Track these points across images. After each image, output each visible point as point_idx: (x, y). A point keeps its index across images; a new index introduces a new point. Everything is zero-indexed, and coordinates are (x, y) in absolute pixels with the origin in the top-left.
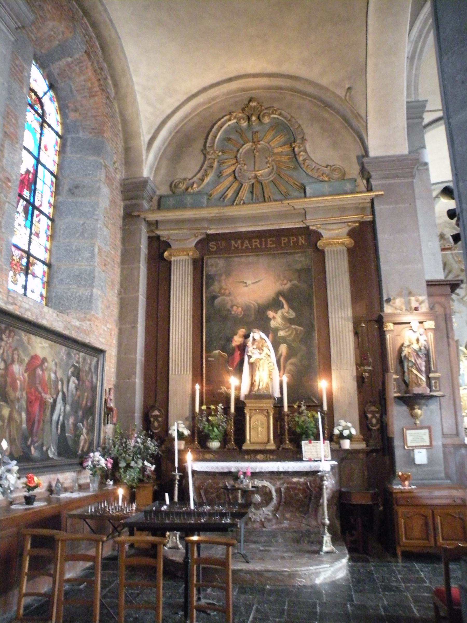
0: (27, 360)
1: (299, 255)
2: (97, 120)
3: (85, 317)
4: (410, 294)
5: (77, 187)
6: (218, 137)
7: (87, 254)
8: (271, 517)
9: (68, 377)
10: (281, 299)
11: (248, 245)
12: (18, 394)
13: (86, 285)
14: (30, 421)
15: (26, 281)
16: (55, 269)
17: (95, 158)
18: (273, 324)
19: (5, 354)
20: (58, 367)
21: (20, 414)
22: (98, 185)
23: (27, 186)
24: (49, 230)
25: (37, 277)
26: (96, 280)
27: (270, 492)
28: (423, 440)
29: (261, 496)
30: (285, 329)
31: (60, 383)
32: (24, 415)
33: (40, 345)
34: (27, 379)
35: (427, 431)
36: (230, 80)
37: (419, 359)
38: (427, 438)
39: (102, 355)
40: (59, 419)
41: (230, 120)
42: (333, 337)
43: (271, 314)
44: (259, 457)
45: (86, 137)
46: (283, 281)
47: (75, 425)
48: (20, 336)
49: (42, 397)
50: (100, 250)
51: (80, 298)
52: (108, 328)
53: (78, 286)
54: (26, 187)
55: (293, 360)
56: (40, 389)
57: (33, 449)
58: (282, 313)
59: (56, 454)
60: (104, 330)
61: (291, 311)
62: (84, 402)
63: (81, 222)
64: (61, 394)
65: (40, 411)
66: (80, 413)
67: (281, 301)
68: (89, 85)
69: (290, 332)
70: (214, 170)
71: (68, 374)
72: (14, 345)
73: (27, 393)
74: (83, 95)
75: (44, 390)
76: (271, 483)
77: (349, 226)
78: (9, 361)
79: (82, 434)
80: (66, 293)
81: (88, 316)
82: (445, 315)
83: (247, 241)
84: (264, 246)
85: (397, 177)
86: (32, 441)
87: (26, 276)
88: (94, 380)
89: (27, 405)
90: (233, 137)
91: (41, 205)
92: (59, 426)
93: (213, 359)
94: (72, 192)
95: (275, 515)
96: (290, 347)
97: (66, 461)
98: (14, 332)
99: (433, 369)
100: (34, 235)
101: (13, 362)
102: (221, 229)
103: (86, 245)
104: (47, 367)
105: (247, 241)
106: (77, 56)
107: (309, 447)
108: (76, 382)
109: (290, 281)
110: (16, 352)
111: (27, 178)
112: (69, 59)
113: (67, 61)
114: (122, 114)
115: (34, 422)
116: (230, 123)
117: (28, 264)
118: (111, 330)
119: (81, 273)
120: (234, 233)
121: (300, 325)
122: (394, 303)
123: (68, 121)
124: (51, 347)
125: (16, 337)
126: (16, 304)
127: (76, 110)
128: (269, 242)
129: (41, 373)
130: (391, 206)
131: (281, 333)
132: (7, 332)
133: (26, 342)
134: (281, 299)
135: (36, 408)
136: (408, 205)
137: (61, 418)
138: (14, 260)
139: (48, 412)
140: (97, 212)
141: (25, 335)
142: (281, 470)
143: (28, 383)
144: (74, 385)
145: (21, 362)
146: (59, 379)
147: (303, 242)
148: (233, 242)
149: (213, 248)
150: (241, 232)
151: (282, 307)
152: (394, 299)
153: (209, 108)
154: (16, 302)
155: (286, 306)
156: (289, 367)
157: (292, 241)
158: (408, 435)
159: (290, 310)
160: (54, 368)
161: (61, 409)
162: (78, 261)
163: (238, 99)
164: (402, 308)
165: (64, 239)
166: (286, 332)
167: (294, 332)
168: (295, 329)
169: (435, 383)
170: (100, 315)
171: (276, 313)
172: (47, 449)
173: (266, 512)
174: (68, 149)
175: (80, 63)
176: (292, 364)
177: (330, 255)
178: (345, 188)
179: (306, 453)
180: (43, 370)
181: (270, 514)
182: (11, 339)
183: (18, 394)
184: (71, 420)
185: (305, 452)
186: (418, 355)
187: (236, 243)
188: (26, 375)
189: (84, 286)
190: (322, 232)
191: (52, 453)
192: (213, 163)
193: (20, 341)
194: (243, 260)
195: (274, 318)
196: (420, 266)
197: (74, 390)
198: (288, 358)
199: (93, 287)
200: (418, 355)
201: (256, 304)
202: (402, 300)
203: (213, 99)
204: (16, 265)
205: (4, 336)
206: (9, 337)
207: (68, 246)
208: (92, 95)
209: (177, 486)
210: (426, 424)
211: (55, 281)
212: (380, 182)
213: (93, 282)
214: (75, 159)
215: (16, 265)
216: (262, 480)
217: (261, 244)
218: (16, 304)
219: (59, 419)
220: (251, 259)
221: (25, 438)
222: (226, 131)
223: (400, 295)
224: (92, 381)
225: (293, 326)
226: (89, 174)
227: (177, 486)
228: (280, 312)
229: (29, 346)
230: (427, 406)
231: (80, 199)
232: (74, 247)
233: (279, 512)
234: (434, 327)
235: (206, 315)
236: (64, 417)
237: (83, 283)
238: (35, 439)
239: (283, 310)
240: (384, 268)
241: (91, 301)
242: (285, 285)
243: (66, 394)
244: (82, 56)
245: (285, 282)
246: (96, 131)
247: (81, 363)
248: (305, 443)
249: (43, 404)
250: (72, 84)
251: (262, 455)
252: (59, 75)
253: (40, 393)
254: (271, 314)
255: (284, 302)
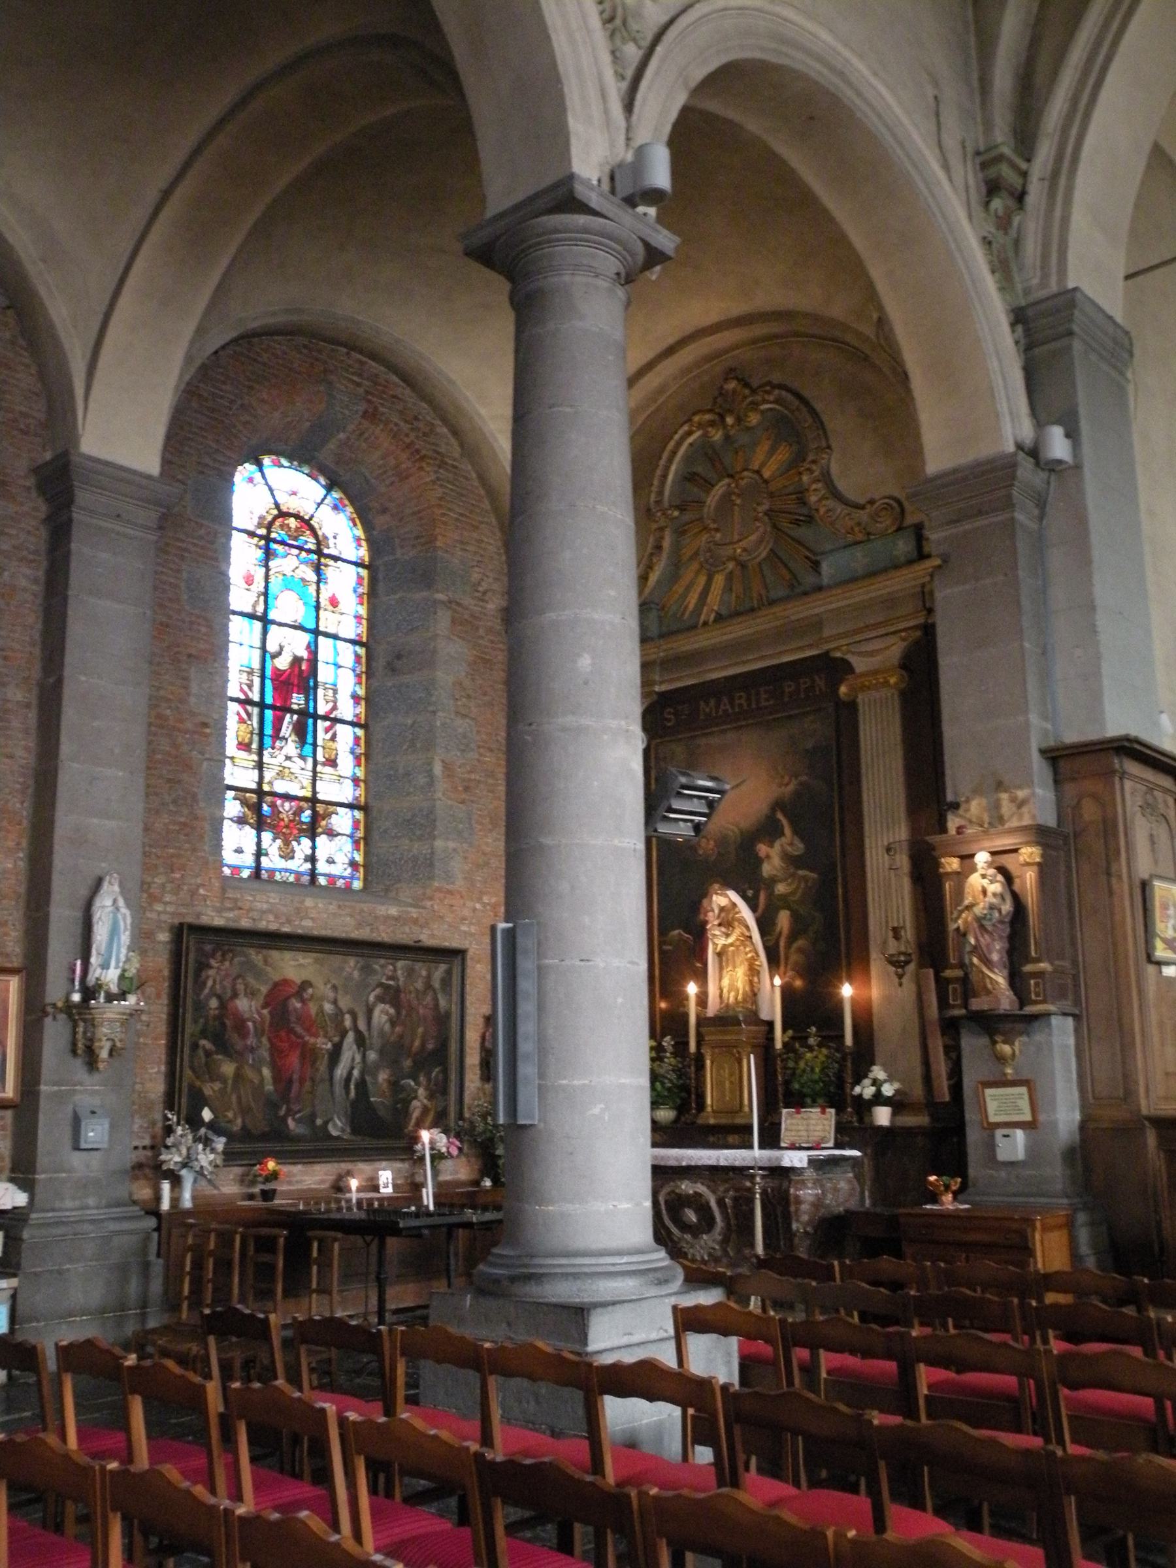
0: (264, 989)
1: (811, 718)
2: (421, 519)
3: (424, 894)
4: (1000, 786)
5: (399, 657)
6: (670, 477)
7: (422, 780)
8: (719, 1253)
9: (367, 1005)
10: (780, 816)
11: (728, 707)
12: (251, 1041)
13: (422, 835)
14: (282, 1079)
15: (314, 848)
16: (374, 813)
17: (425, 594)
18: (767, 870)
19: (218, 987)
20: (340, 992)
21: (260, 1072)
22: (433, 644)
23: (298, 686)
24: (358, 745)
25: (339, 834)
26: (438, 823)
27: (708, 1203)
28: (1019, 1111)
29: (696, 1212)
30: (786, 880)
31: (347, 1017)
32: (266, 1072)
33: (292, 963)
34: (268, 1017)
35: (1023, 1090)
36: (670, 351)
37: (986, 936)
38: (1025, 1104)
39: (460, 957)
40: (350, 1074)
41: (689, 433)
42: (873, 889)
43: (762, 849)
44: (731, 1139)
45: (406, 557)
46: (782, 777)
47: (394, 1085)
48: (246, 956)
49: (305, 1044)
50: (446, 766)
51: (415, 859)
52: (484, 905)
53: (411, 841)
54: (295, 689)
55: (800, 943)
56: (299, 1030)
57: (291, 1123)
58: (782, 846)
59: (348, 1130)
60: (475, 910)
61: (797, 841)
62: (417, 1043)
63: (410, 722)
64: (350, 1037)
65: (302, 1064)
66: (408, 1063)
67: (779, 820)
68: (393, 462)
69: (794, 886)
70: (665, 555)
71: (367, 1001)
72: (235, 971)
73: (269, 1039)
74: (387, 482)
75: (308, 1030)
76: (708, 1187)
77: (903, 639)
78: (229, 993)
79: (415, 1098)
80: (393, 854)
81: (429, 892)
82: (1104, 821)
83: (725, 700)
84: (754, 706)
85: (980, 513)
86: (289, 1111)
87: (313, 841)
88: (442, 1003)
89: (272, 1055)
90: (699, 469)
91: (335, 708)
92: (352, 1087)
93: (669, 948)
94: (392, 669)
95: (725, 1251)
96: (796, 917)
97: (369, 1142)
98: (231, 951)
99: (1033, 954)
100: (324, 764)
101: (235, 995)
102: (678, 679)
103: (419, 763)
104: (312, 996)
105: (725, 700)
106: (351, 427)
107: (794, 1121)
108: (392, 1011)
109: (796, 777)
110: (240, 981)
111: (296, 671)
112: (342, 436)
113: (340, 440)
114: (482, 478)
115: (290, 1081)
116: (691, 440)
117: (315, 818)
118: (494, 907)
119: (414, 816)
120: (704, 683)
121: (812, 870)
122: (968, 810)
123: (375, 533)
124: (316, 960)
125: (236, 960)
126: (240, 909)
127: (384, 511)
128: (764, 696)
129: (298, 1005)
130: (967, 587)
131: (781, 888)
132: (219, 954)
133: (261, 964)
134: (780, 816)
135: (294, 1060)
136: (1001, 577)
137: (356, 1073)
138: (283, 820)
139: (323, 1066)
140: (434, 699)
141: (258, 953)
142: (723, 1163)
143: (271, 1025)
144: (385, 1018)
145: (252, 993)
146: (345, 1010)
147: (824, 689)
148: (702, 703)
149: (669, 720)
150: (713, 681)
151: (782, 834)
152: (968, 801)
153: (657, 410)
154: (239, 904)
155: (788, 831)
156: (794, 957)
157: (803, 686)
158: (988, 1100)
159: (788, 842)
160: (331, 995)
161: (353, 1059)
162: (408, 794)
163: (706, 378)
164: (983, 822)
165: (385, 756)
166: (789, 885)
167: (803, 885)
168: (804, 877)
169: (1037, 984)
170: (460, 884)
171: (772, 846)
172: (326, 1123)
173: (711, 1244)
174: (381, 587)
175: (361, 434)
176: (800, 950)
177: (867, 708)
178: (895, 553)
179: (788, 1133)
180: (303, 1001)
181: (717, 1247)
182: (227, 963)
183: (462, 725)
184: (383, 1076)
185: (786, 1129)
186: (982, 927)
187: (707, 703)
188: (265, 1012)
189: (420, 838)
190: (854, 660)
191: (337, 1127)
192: (662, 538)
193: (250, 966)
194: (715, 741)
195: (768, 857)
196: (1021, 718)
197: (387, 1027)
198: (793, 936)
199: (434, 838)
200: (982, 927)
201: (736, 830)
202: (984, 801)
203: (661, 390)
204: (287, 827)
205: (213, 962)
206: (222, 962)
207: (391, 768)
208: (403, 477)
209: (758, 1196)
210: (1025, 1075)
211: (376, 836)
212: (943, 534)
213: (434, 828)
214: (393, 603)
215: (287, 827)
216: (696, 1182)
217: (749, 699)
218: (240, 909)
219: (350, 1074)
220: (731, 736)
221: (273, 1106)
222: (688, 459)
223: (977, 791)
224: (437, 1005)
225: (801, 872)
226: (417, 627)
227: (758, 1196)
228: (777, 846)
229: (269, 969)
230: (1028, 1035)
231: (406, 679)
232: (401, 771)
233: (731, 1244)
234: (1038, 860)
235: (658, 860)
236: (362, 1073)
237: (418, 833)
238: (295, 1107)
239: (783, 839)
240: (949, 732)
241: (431, 865)
242: (787, 784)
243: (366, 1034)
244: (360, 424)
245: (786, 779)
246: (422, 540)
247: (402, 979)
248: (788, 1113)
249: (309, 1055)
250: (363, 470)
251: (736, 1137)
252: (337, 463)
253: (300, 1037)
254: (762, 849)
255: (785, 822)
